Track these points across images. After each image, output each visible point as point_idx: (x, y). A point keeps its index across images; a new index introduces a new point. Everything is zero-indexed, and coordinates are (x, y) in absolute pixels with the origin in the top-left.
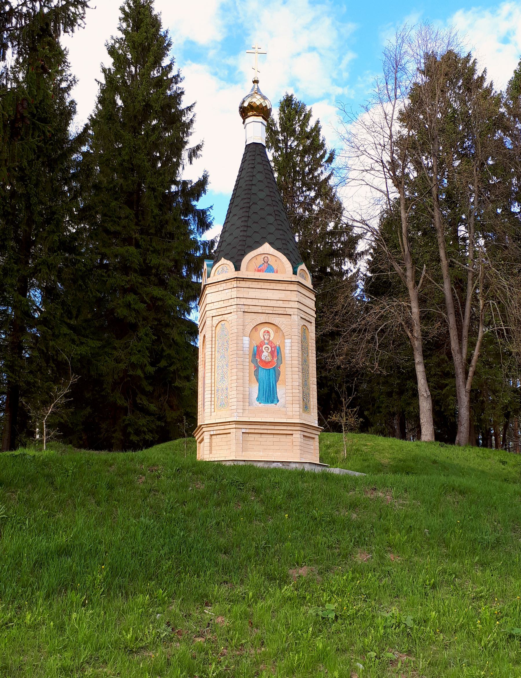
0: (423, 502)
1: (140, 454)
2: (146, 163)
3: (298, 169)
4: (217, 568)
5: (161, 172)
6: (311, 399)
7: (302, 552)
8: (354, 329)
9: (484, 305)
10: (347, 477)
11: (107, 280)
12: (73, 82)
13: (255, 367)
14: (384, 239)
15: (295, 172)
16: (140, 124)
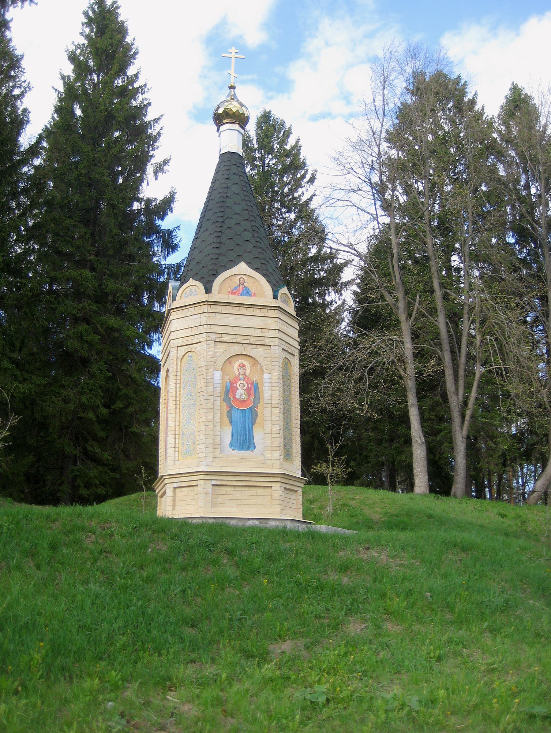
0: (423, 561)
1: (90, 509)
2: (105, 178)
3: (276, 189)
4: (182, 645)
5: (122, 187)
6: (294, 445)
7: (286, 624)
8: (341, 366)
9: (482, 342)
10: (336, 536)
11: (56, 308)
12: (27, 89)
13: (228, 407)
14: (543, 282)
15: (273, 192)
16: (101, 136)
